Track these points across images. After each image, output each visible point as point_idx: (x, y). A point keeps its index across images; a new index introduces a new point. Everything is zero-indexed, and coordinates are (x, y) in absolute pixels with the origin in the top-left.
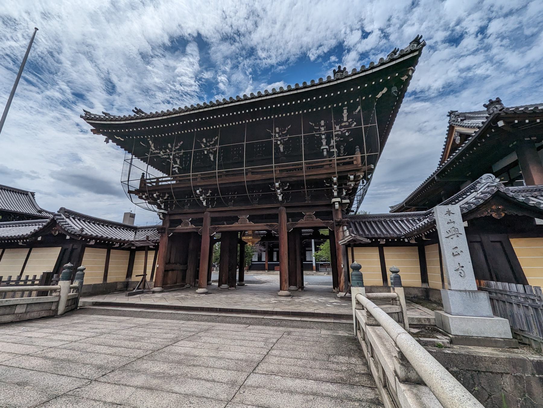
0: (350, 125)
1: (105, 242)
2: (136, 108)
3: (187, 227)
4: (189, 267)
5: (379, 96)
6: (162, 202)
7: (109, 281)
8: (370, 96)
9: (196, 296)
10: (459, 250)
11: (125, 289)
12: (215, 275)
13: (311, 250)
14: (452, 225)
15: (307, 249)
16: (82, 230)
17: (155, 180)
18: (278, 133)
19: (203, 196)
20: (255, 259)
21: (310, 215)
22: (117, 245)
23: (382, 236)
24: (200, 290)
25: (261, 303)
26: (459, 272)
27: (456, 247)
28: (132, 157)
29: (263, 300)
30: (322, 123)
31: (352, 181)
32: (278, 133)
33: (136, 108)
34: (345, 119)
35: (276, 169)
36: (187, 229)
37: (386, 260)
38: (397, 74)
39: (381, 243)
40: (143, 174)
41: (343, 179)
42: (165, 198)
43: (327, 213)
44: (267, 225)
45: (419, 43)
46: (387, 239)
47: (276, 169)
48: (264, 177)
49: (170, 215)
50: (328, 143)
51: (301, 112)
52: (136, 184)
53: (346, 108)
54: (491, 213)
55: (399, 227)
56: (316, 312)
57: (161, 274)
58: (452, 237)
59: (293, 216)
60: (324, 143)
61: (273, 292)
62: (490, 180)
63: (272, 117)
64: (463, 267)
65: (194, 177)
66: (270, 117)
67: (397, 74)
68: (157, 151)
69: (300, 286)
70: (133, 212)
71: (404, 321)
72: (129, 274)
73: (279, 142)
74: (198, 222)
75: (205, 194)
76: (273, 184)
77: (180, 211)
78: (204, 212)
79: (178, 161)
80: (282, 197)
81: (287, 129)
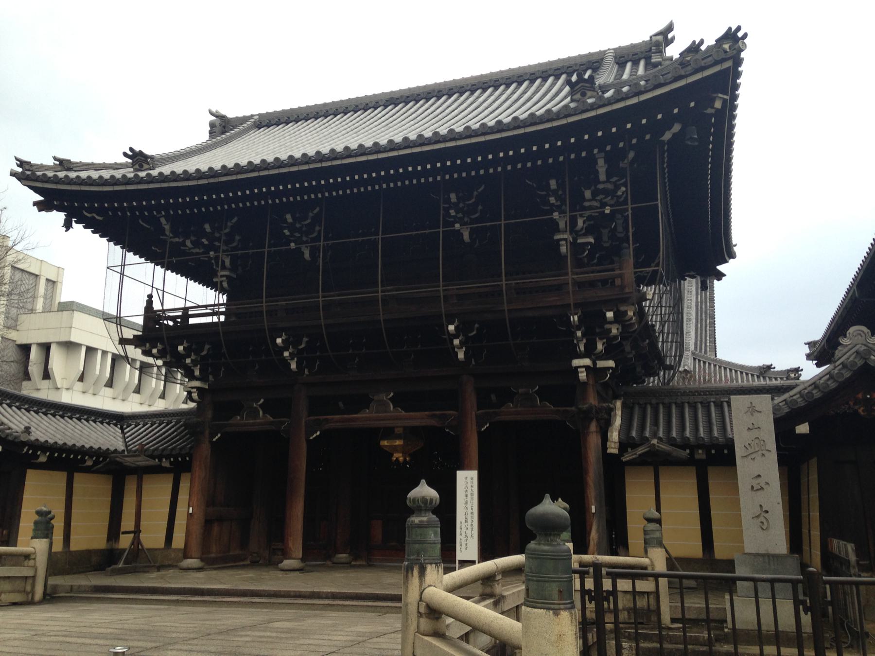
2: (131, 149)
5: (667, 136)
7: (74, 547)
9: (280, 574)
10: (762, 481)
14: (755, 433)
16: (27, 430)
18: (456, 205)
19: (291, 350)
24: (287, 563)
27: (759, 476)
28: (124, 258)
30: (553, 184)
31: (611, 323)
34: (602, 177)
40: (150, 297)
54: (856, 407)
57: (197, 529)
58: (753, 456)
62: (860, 340)
68: (177, 240)
72: (114, 531)
76: (443, 329)
80: (465, 354)
81: (475, 193)
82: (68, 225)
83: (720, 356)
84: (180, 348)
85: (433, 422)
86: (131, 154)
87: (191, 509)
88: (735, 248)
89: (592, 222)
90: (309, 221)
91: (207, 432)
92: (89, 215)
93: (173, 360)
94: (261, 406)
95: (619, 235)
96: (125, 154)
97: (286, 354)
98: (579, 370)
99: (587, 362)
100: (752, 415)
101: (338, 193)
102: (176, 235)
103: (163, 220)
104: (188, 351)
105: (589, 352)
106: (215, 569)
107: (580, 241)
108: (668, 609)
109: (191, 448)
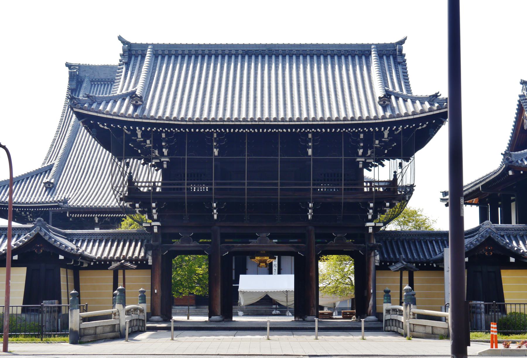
31: (387, 207)
44: (293, 246)
83: (9, 178)
88: (447, 188)
99: (372, 224)
102: (142, 138)
107: (367, 161)
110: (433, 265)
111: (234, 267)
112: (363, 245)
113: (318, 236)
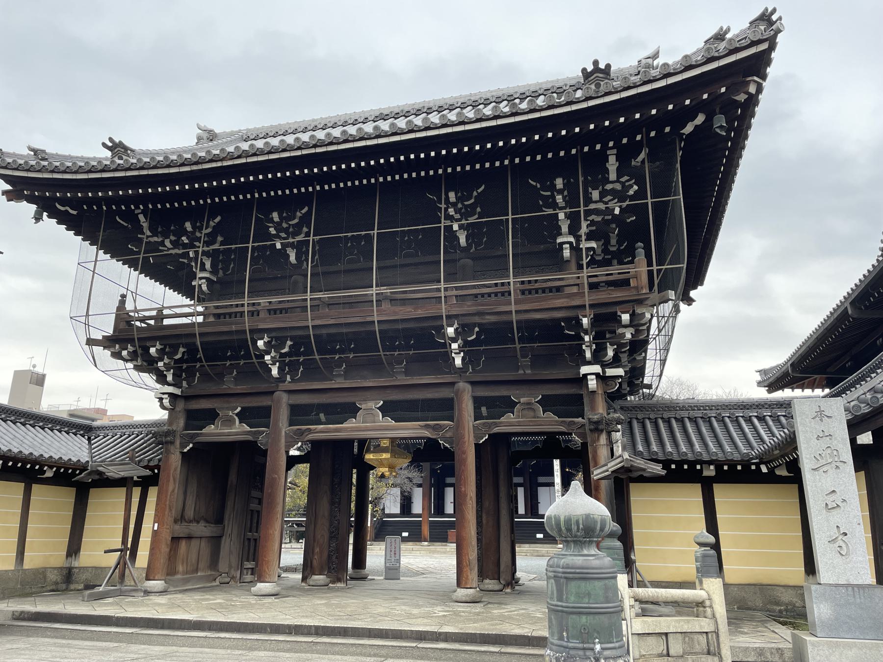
0: (625, 188)
1: (24, 465)
2: (111, 139)
3: (230, 429)
4: (228, 530)
5: (689, 128)
6: (168, 367)
8: (667, 129)
9: (253, 600)
10: (838, 498)
11: (64, 586)
12: (293, 554)
13: (552, 484)
15: (541, 479)
17: (154, 313)
18: (454, 205)
19: (273, 354)
20: (392, 506)
21: (529, 404)
22: (49, 474)
23: (705, 457)
24: (262, 587)
25: (410, 616)
26: (837, 544)
27: (834, 491)
29: (415, 611)
30: (559, 183)
31: (626, 326)
32: (454, 205)
33: (111, 139)
34: (613, 176)
35: (449, 293)
36: (229, 435)
37: (719, 516)
38: (723, 90)
39: (706, 473)
40: (123, 296)
41: (605, 322)
42: (177, 357)
43: (570, 400)
44: (427, 426)
45: (771, 23)
46: (719, 465)
47: (449, 293)
48: (420, 313)
49: (186, 398)
50: (574, 230)
51: (506, 162)
52: (106, 326)
53: (615, 151)
55: (750, 436)
56: (535, 634)
58: (825, 469)
59: (492, 407)
60: (565, 228)
61: (443, 596)
63: (440, 171)
64: (845, 534)
65: (251, 309)
66: (436, 172)
67: (723, 90)
68: (156, 239)
69: (509, 578)
70: (39, 370)
71: (719, 654)
73: (456, 227)
74: (257, 416)
75: (278, 348)
76: (440, 329)
77: (212, 389)
78: (273, 393)
79: (208, 265)
80: (463, 359)
81: (475, 193)
82: (38, 218)
84: (153, 350)
85: (427, 434)
86: (110, 144)
87: (156, 525)
89: (594, 228)
90: (296, 221)
91: (178, 442)
92: (62, 208)
93: (145, 364)
94: (237, 415)
95: (612, 249)
96: (104, 145)
97: (267, 358)
98: (589, 377)
100: (821, 420)
101: (330, 186)
102: (155, 234)
103: (141, 218)
104: (161, 352)
105: (597, 358)
106: (181, 592)
108: (729, 653)
109: (160, 460)
110: (758, 469)
111: (354, 481)
112: (580, 419)
113: (478, 402)
